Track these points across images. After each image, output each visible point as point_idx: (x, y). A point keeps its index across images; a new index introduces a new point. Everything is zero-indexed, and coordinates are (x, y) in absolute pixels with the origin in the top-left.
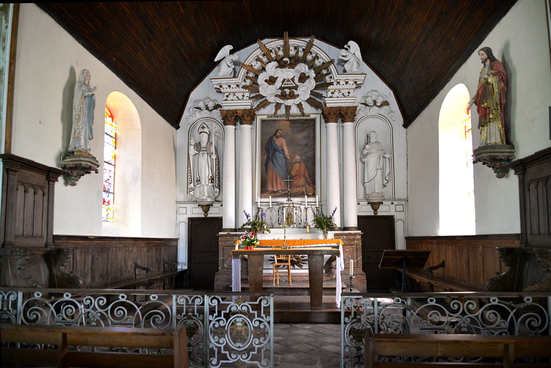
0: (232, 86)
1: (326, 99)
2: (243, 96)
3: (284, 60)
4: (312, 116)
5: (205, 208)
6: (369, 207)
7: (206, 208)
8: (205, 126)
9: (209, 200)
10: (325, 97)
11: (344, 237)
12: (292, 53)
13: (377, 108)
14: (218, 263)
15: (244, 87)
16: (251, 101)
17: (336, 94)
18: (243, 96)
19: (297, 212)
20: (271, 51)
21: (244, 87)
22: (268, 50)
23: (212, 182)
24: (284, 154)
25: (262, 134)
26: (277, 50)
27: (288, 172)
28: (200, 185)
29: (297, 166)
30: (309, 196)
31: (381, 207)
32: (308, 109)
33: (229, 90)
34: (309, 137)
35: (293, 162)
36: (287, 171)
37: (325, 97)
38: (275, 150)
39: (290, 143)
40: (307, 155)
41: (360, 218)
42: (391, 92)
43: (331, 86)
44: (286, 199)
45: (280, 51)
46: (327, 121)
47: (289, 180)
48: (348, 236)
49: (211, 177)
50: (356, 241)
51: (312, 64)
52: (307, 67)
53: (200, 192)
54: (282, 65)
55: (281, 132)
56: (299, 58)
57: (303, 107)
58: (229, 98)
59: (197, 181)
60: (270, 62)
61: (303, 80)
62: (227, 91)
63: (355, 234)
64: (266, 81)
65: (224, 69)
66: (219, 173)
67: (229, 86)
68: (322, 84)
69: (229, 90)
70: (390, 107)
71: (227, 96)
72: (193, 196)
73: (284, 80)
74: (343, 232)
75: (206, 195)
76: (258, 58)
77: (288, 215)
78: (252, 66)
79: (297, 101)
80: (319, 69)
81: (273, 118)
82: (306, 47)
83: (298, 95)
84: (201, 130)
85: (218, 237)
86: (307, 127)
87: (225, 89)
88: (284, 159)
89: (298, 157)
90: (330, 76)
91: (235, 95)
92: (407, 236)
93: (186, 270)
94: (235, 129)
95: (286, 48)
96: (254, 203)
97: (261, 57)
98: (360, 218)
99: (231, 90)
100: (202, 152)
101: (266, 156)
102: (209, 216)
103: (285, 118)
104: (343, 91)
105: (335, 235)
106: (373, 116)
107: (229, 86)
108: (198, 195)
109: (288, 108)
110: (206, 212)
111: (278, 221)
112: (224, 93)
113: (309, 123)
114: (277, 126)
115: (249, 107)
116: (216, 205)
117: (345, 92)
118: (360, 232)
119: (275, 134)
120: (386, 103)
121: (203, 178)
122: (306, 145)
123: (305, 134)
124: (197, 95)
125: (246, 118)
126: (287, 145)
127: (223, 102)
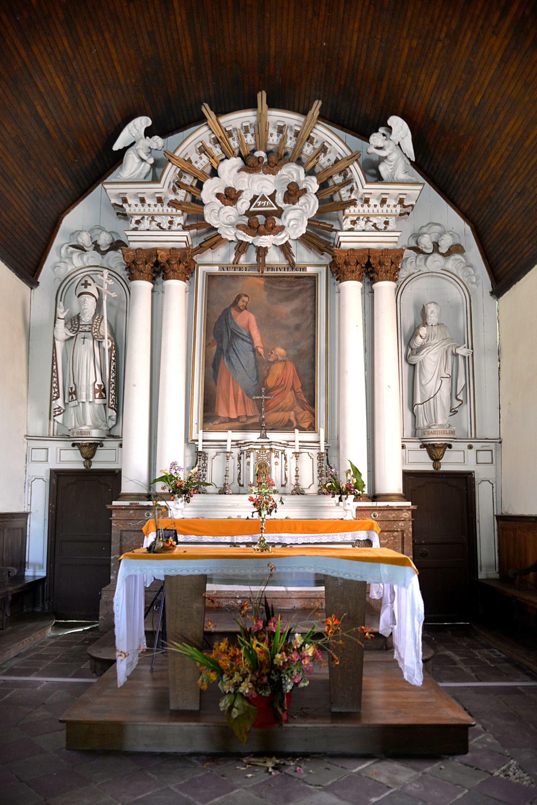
0: (148, 201)
1: (340, 234)
2: (171, 222)
3: (257, 154)
4: (310, 270)
5: (85, 450)
6: (424, 455)
7: (89, 449)
8: (90, 281)
9: (95, 433)
10: (336, 231)
11: (377, 514)
12: (274, 140)
13: (440, 257)
14: (109, 566)
15: (173, 204)
16: (186, 233)
17: (361, 224)
18: (171, 222)
19: (279, 460)
20: (230, 134)
21: (173, 204)
22: (224, 130)
23: (101, 397)
24: (252, 343)
25: (209, 302)
26: (242, 132)
27: (261, 380)
28: (76, 403)
29: (277, 370)
30: (302, 430)
31: (448, 453)
32: (304, 256)
33: (140, 209)
34: (303, 311)
35: (271, 360)
36: (257, 378)
37: (336, 231)
38: (235, 335)
39: (267, 321)
40: (298, 347)
41: (408, 476)
42: (468, 228)
43: (352, 208)
44: (258, 435)
45: (249, 135)
46: (341, 279)
47: (263, 397)
48: (385, 513)
49: (100, 386)
50: (401, 524)
51: (311, 165)
52: (302, 171)
53: (77, 416)
54: (250, 164)
55: (246, 299)
56: (286, 154)
57: (293, 250)
58: (142, 227)
59: (70, 394)
60: (227, 158)
61: (293, 198)
62: (137, 211)
63: (400, 509)
64: (218, 196)
65: (133, 166)
66: (117, 378)
67: (143, 200)
68: (331, 204)
69: (140, 209)
70: (465, 257)
71: (138, 222)
72: (63, 424)
73: (255, 197)
74: (374, 504)
75: (89, 422)
76: (203, 145)
77: (260, 466)
78: (189, 161)
79: (281, 239)
80: (328, 174)
81: (232, 272)
82: (302, 128)
83: (282, 228)
84: (82, 289)
85: (110, 512)
86: (300, 291)
87: (133, 207)
88: (252, 354)
89: (280, 351)
90: (349, 187)
91: (153, 220)
92: (499, 513)
93: (43, 580)
94: (153, 291)
95: (260, 130)
96: (190, 442)
97: (209, 145)
98: (406, 475)
99: (145, 209)
100: (83, 334)
101: (215, 348)
102: (94, 466)
103: (255, 272)
104: (374, 220)
105: (359, 510)
106: (431, 274)
107: (143, 200)
108: (72, 423)
109: (262, 252)
110: (88, 458)
111: (239, 479)
112: (132, 215)
113: (305, 284)
114: (240, 287)
115: (183, 245)
116: (109, 444)
117: (379, 222)
118: (409, 504)
119: (235, 303)
120: (456, 249)
121: (84, 388)
122: (297, 327)
123: (296, 304)
124: (78, 220)
125: (175, 266)
126: (259, 327)
127: (128, 233)
